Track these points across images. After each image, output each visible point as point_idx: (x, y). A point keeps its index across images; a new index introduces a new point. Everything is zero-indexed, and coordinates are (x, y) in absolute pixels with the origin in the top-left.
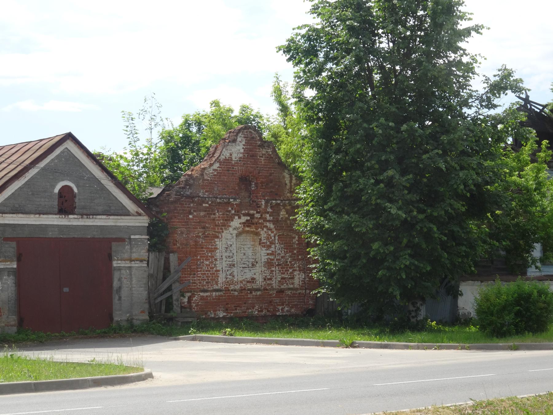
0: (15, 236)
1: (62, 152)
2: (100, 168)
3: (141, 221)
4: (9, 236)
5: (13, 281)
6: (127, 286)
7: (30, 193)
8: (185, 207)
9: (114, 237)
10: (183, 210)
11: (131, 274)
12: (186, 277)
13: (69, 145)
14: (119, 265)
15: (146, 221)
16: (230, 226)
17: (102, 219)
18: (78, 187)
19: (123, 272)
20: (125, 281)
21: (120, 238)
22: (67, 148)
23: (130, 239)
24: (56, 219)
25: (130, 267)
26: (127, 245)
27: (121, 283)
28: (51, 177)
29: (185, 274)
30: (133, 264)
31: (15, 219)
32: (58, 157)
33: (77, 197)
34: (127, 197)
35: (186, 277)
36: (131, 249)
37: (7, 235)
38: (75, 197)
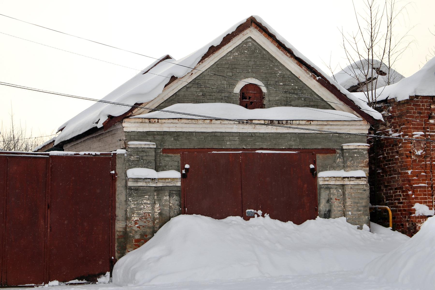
0: (178, 147)
1: (245, 42)
2: (296, 61)
3: (358, 127)
4: (170, 147)
5: (177, 202)
6: (339, 209)
7: (201, 94)
8: (422, 109)
9: (320, 147)
10: (420, 113)
11: (344, 194)
12: (426, 198)
13: (253, 33)
14: (326, 183)
15: (365, 127)
16: (97, 281)
17: (78, 143)
18: (267, 86)
19: (333, 191)
20: (336, 203)
21: (329, 148)
22: (250, 38)
23: (342, 150)
24: (235, 126)
25: (343, 185)
26: (339, 157)
27: (331, 206)
28: (230, 74)
29: (425, 195)
30: (346, 182)
31: (178, 125)
32: (238, 48)
33: (267, 99)
34: (335, 97)
35: (426, 198)
36: (344, 162)
37: (167, 146)
38: (263, 98)
